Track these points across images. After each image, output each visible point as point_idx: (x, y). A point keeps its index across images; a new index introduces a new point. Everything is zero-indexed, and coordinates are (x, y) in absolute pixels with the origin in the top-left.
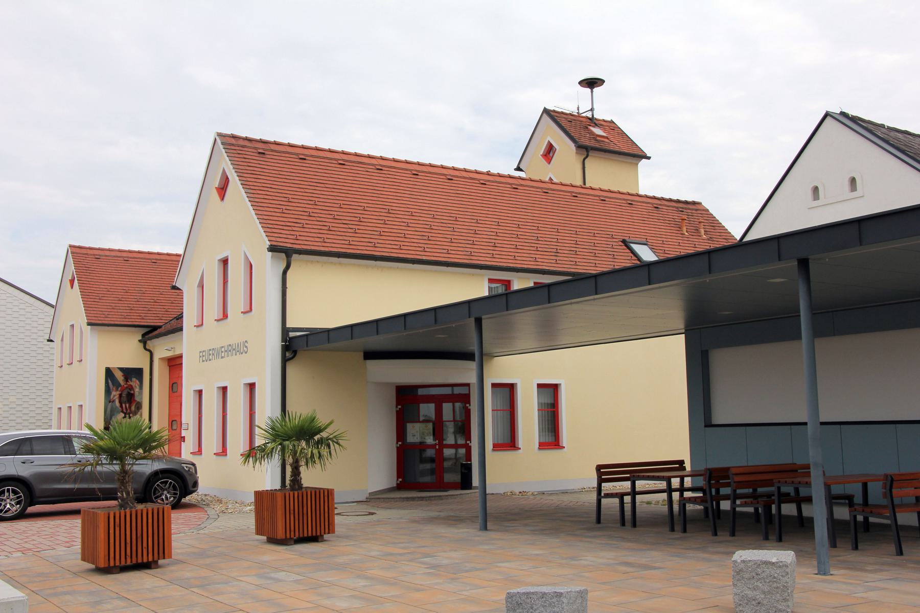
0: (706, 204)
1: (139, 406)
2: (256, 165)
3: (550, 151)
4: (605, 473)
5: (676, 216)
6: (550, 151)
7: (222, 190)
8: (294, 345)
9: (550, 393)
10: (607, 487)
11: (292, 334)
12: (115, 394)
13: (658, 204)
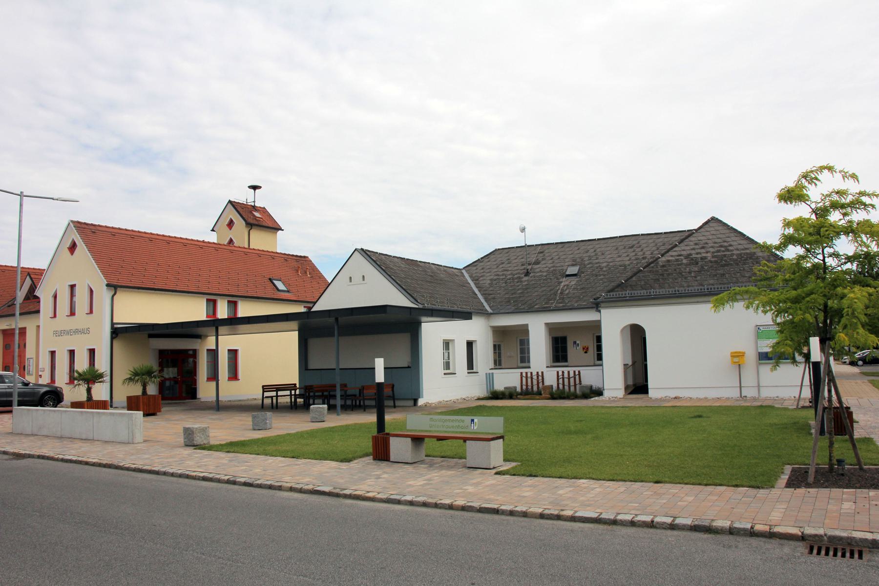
0: (310, 258)
2: (90, 236)
3: (231, 224)
4: (265, 388)
5: (295, 264)
6: (231, 224)
7: (73, 248)
8: (117, 332)
9: (233, 354)
10: (266, 394)
11: (116, 326)
13: (288, 258)
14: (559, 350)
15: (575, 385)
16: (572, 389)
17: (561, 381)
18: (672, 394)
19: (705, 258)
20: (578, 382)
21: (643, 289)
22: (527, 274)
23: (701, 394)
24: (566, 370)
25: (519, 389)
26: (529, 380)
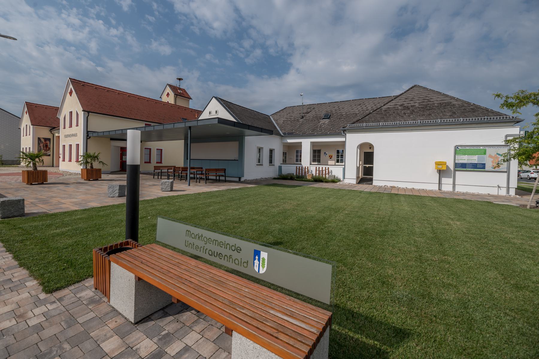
1: (49, 149)
2: (80, 87)
10: (156, 171)
12: (42, 145)
14: (316, 155)
15: (326, 174)
16: (324, 176)
17: (318, 172)
18: (389, 184)
19: (414, 106)
20: (327, 172)
21: (373, 122)
22: (303, 117)
23: (410, 186)
24: (321, 166)
25: (295, 174)
26: (301, 170)
